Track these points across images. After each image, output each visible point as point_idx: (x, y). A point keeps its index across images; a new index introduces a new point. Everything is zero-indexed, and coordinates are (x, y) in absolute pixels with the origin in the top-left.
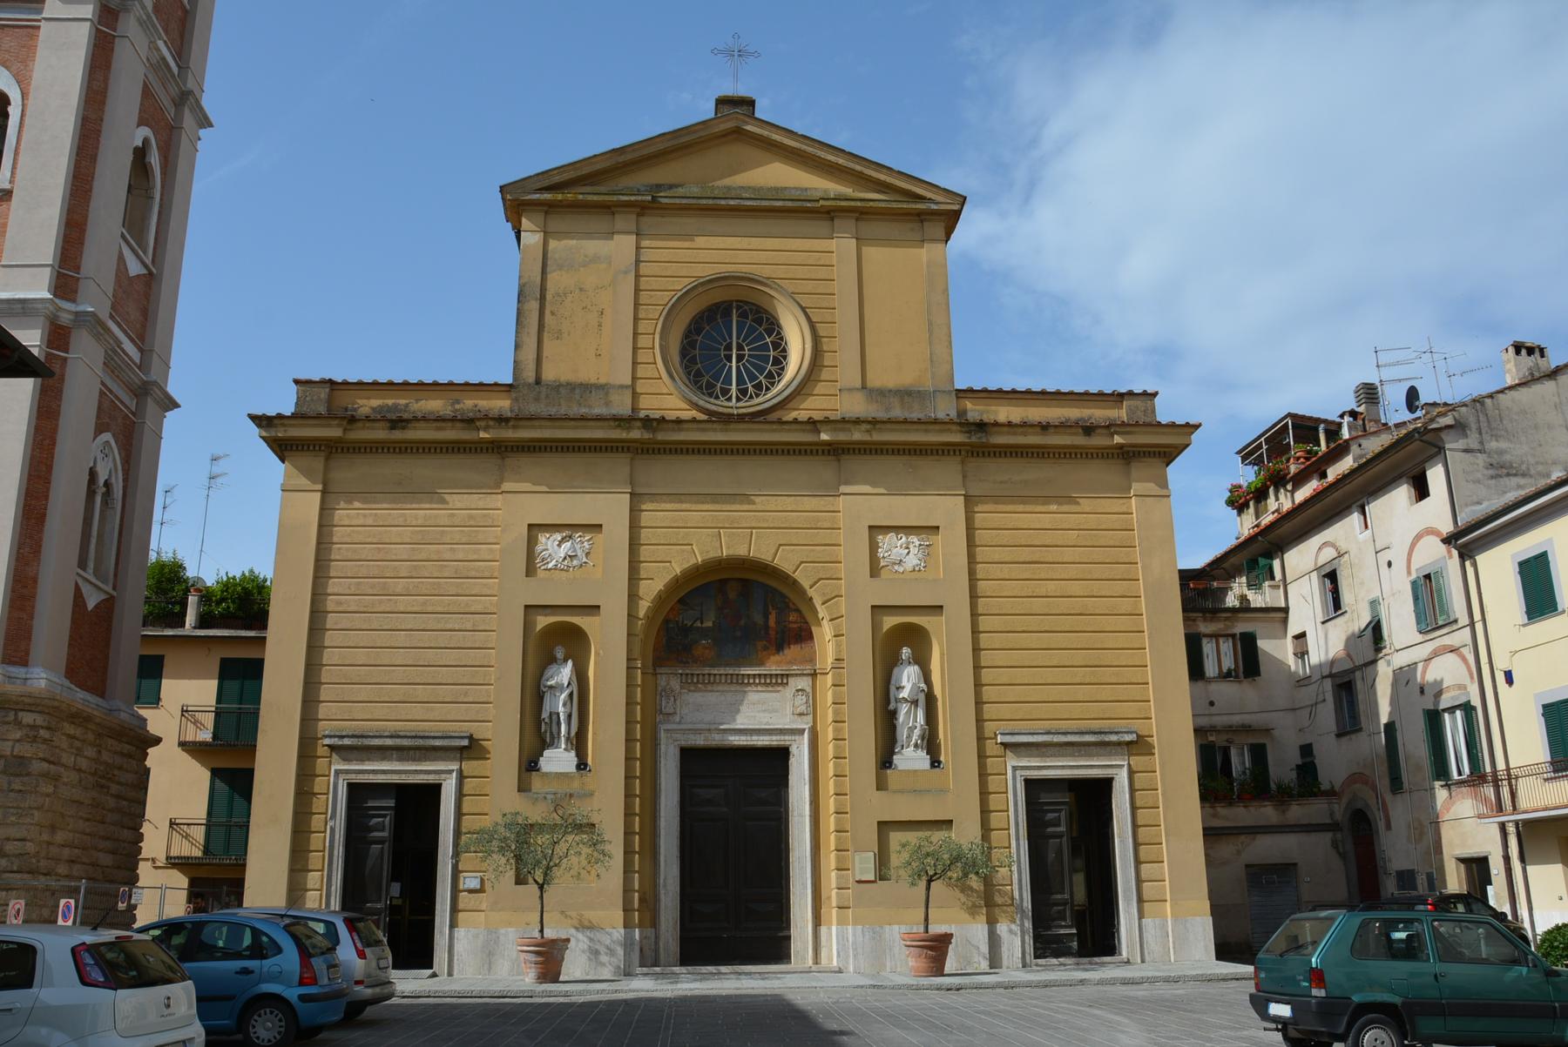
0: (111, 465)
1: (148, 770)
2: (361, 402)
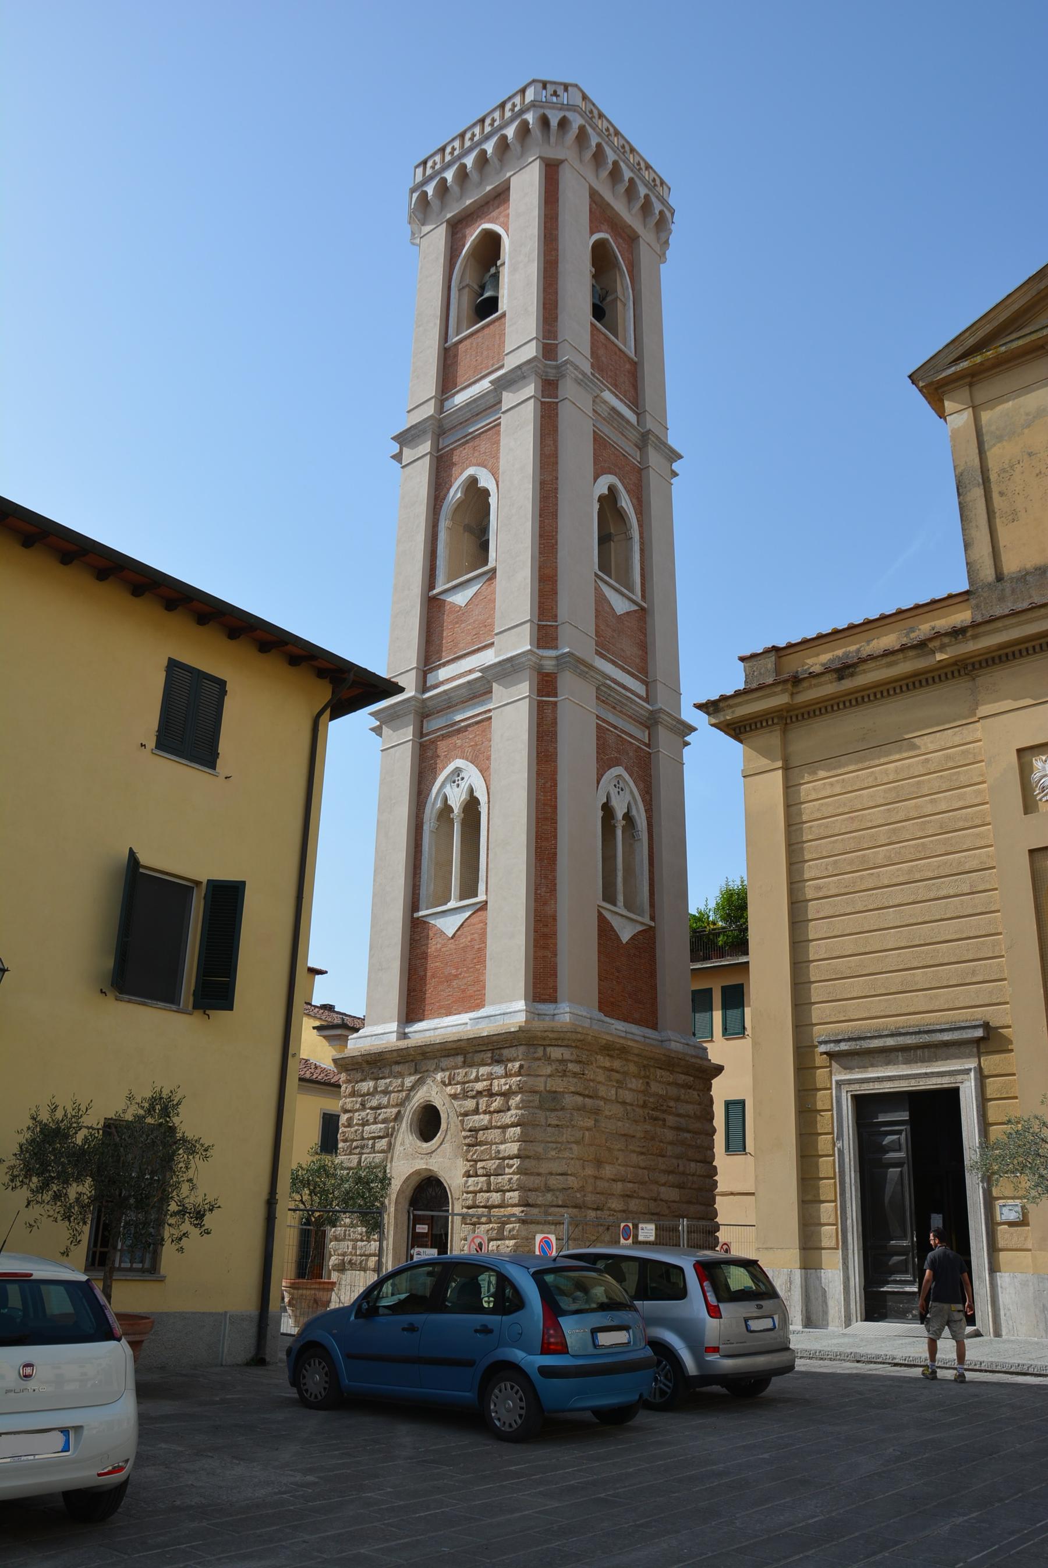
0: (628, 797)
2: (809, 661)
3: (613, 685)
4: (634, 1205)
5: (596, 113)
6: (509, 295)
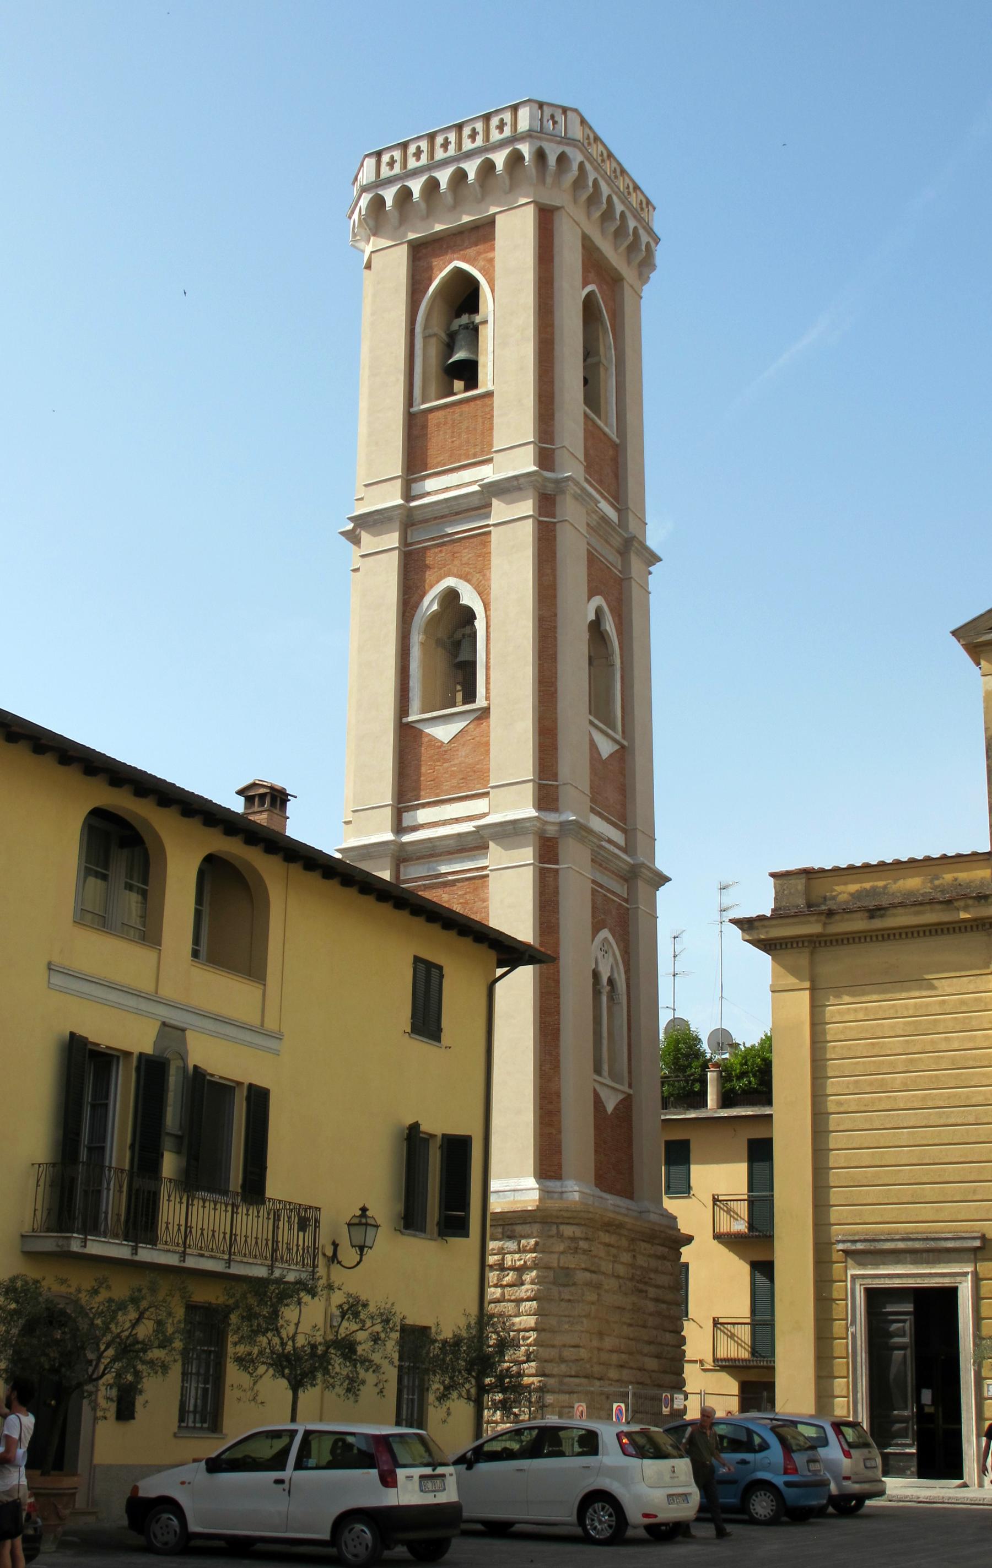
0: (611, 960)
1: (686, 1266)
5: (592, 136)
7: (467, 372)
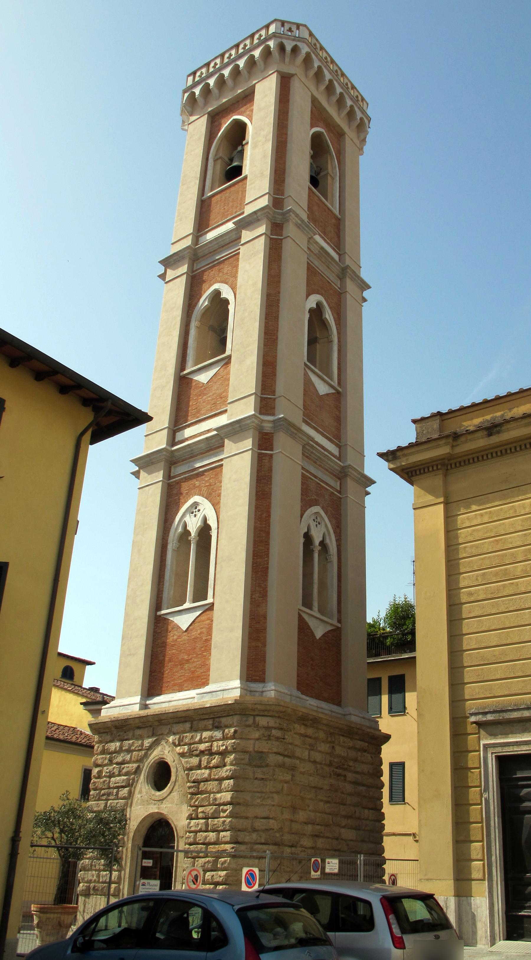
0: (323, 530)
2: (465, 424)
3: (315, 445)
4: (320, 843)
6: (250, 164)
7: (237, 171)
